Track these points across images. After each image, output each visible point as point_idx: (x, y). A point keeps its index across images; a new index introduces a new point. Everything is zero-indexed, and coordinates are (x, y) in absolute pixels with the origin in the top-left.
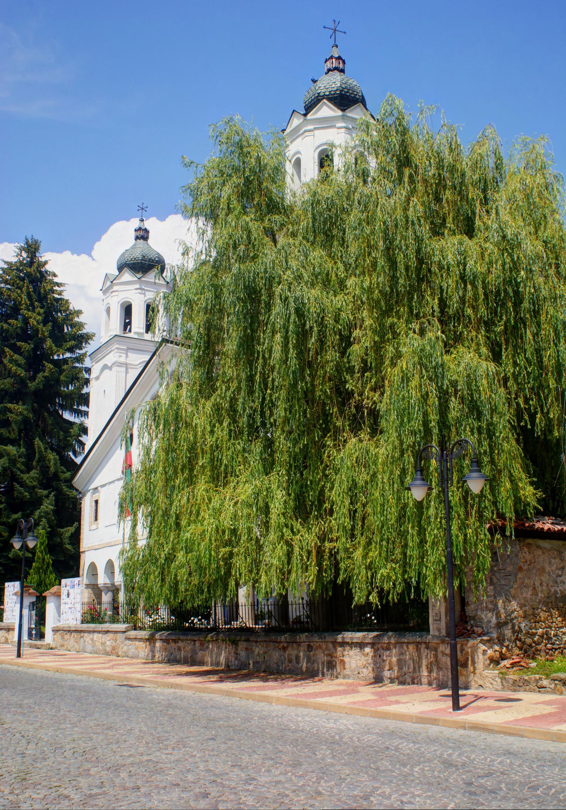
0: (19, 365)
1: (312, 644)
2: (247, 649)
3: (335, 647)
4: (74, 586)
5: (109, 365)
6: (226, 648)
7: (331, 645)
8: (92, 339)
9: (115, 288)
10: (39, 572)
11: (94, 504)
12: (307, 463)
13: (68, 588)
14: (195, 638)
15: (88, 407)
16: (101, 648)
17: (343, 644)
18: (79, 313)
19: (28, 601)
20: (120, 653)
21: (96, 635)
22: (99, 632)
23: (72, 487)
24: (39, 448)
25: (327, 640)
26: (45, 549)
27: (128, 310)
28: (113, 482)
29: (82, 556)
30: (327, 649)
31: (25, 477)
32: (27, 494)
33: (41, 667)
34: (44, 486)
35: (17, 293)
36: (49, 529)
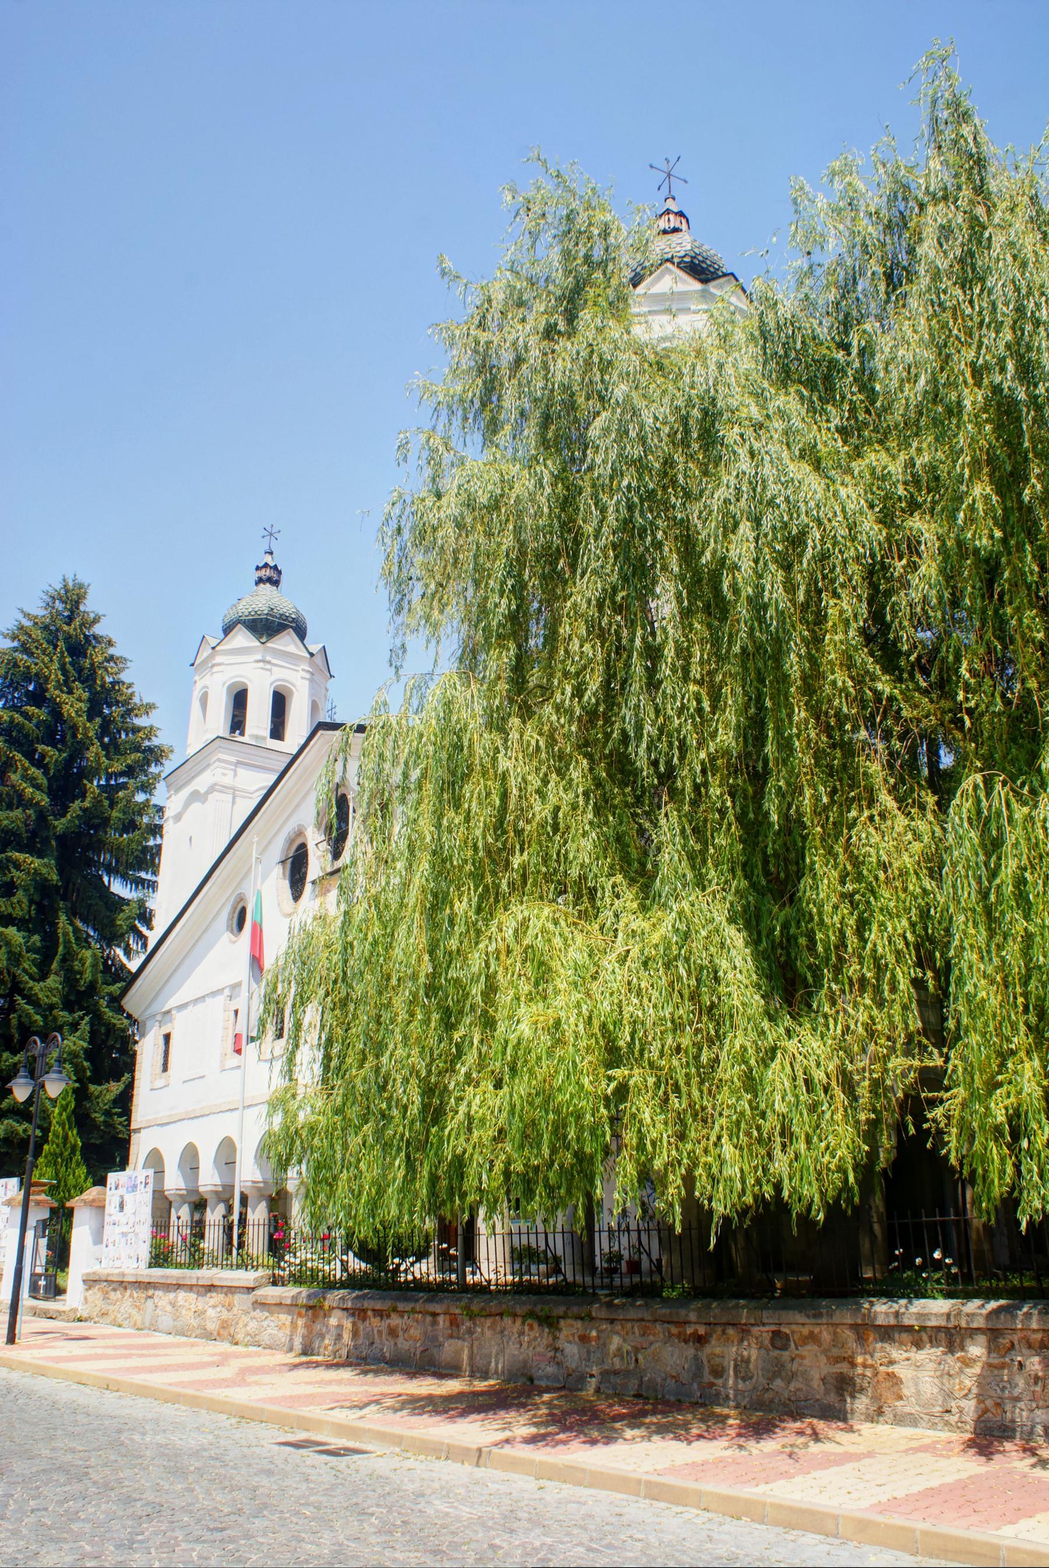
0: (37, 787)
1: (785, 1330)
2: (584, 1339)
3: (861, 1339)
4: (135, 1186)
5: (202, 791)
6: (521, 1333)
7: (849, 1335)
8: (167, 757)
9: (218, 659)
10: (55, 1164)
11: (161, 1041)
12: (770, 879)
13: (122, 1191)
14: (437, 1308)
15: (155, 873)
16: (194, 1323)
17: (888, 1333)
18: (149, 708)
19: (38, 1215)
20: (239, 1337)
21: (182, 1295)
22: (190, 1288)
23: (120, 1010)
24: (66, 934)
25: (836, 1319)
26: (69, 1118)
27: (240, 700)
28: (203, 998)
29: (134, 1138)
30: (836, 1341)
31: (37, 987)
32: (38, 1017)
33: (67, 1375)
34: (69, 1006)
35: (43, 661)
36: (77, 1085)
